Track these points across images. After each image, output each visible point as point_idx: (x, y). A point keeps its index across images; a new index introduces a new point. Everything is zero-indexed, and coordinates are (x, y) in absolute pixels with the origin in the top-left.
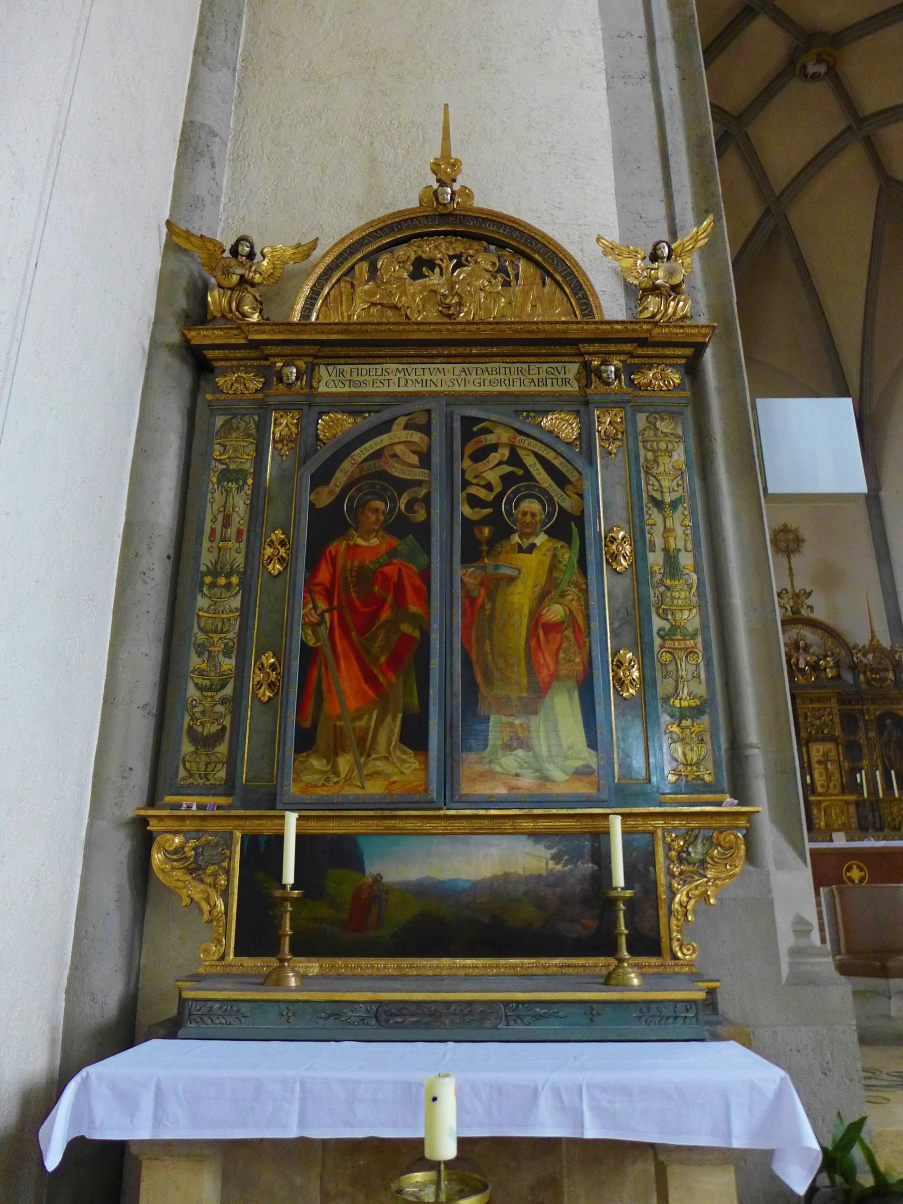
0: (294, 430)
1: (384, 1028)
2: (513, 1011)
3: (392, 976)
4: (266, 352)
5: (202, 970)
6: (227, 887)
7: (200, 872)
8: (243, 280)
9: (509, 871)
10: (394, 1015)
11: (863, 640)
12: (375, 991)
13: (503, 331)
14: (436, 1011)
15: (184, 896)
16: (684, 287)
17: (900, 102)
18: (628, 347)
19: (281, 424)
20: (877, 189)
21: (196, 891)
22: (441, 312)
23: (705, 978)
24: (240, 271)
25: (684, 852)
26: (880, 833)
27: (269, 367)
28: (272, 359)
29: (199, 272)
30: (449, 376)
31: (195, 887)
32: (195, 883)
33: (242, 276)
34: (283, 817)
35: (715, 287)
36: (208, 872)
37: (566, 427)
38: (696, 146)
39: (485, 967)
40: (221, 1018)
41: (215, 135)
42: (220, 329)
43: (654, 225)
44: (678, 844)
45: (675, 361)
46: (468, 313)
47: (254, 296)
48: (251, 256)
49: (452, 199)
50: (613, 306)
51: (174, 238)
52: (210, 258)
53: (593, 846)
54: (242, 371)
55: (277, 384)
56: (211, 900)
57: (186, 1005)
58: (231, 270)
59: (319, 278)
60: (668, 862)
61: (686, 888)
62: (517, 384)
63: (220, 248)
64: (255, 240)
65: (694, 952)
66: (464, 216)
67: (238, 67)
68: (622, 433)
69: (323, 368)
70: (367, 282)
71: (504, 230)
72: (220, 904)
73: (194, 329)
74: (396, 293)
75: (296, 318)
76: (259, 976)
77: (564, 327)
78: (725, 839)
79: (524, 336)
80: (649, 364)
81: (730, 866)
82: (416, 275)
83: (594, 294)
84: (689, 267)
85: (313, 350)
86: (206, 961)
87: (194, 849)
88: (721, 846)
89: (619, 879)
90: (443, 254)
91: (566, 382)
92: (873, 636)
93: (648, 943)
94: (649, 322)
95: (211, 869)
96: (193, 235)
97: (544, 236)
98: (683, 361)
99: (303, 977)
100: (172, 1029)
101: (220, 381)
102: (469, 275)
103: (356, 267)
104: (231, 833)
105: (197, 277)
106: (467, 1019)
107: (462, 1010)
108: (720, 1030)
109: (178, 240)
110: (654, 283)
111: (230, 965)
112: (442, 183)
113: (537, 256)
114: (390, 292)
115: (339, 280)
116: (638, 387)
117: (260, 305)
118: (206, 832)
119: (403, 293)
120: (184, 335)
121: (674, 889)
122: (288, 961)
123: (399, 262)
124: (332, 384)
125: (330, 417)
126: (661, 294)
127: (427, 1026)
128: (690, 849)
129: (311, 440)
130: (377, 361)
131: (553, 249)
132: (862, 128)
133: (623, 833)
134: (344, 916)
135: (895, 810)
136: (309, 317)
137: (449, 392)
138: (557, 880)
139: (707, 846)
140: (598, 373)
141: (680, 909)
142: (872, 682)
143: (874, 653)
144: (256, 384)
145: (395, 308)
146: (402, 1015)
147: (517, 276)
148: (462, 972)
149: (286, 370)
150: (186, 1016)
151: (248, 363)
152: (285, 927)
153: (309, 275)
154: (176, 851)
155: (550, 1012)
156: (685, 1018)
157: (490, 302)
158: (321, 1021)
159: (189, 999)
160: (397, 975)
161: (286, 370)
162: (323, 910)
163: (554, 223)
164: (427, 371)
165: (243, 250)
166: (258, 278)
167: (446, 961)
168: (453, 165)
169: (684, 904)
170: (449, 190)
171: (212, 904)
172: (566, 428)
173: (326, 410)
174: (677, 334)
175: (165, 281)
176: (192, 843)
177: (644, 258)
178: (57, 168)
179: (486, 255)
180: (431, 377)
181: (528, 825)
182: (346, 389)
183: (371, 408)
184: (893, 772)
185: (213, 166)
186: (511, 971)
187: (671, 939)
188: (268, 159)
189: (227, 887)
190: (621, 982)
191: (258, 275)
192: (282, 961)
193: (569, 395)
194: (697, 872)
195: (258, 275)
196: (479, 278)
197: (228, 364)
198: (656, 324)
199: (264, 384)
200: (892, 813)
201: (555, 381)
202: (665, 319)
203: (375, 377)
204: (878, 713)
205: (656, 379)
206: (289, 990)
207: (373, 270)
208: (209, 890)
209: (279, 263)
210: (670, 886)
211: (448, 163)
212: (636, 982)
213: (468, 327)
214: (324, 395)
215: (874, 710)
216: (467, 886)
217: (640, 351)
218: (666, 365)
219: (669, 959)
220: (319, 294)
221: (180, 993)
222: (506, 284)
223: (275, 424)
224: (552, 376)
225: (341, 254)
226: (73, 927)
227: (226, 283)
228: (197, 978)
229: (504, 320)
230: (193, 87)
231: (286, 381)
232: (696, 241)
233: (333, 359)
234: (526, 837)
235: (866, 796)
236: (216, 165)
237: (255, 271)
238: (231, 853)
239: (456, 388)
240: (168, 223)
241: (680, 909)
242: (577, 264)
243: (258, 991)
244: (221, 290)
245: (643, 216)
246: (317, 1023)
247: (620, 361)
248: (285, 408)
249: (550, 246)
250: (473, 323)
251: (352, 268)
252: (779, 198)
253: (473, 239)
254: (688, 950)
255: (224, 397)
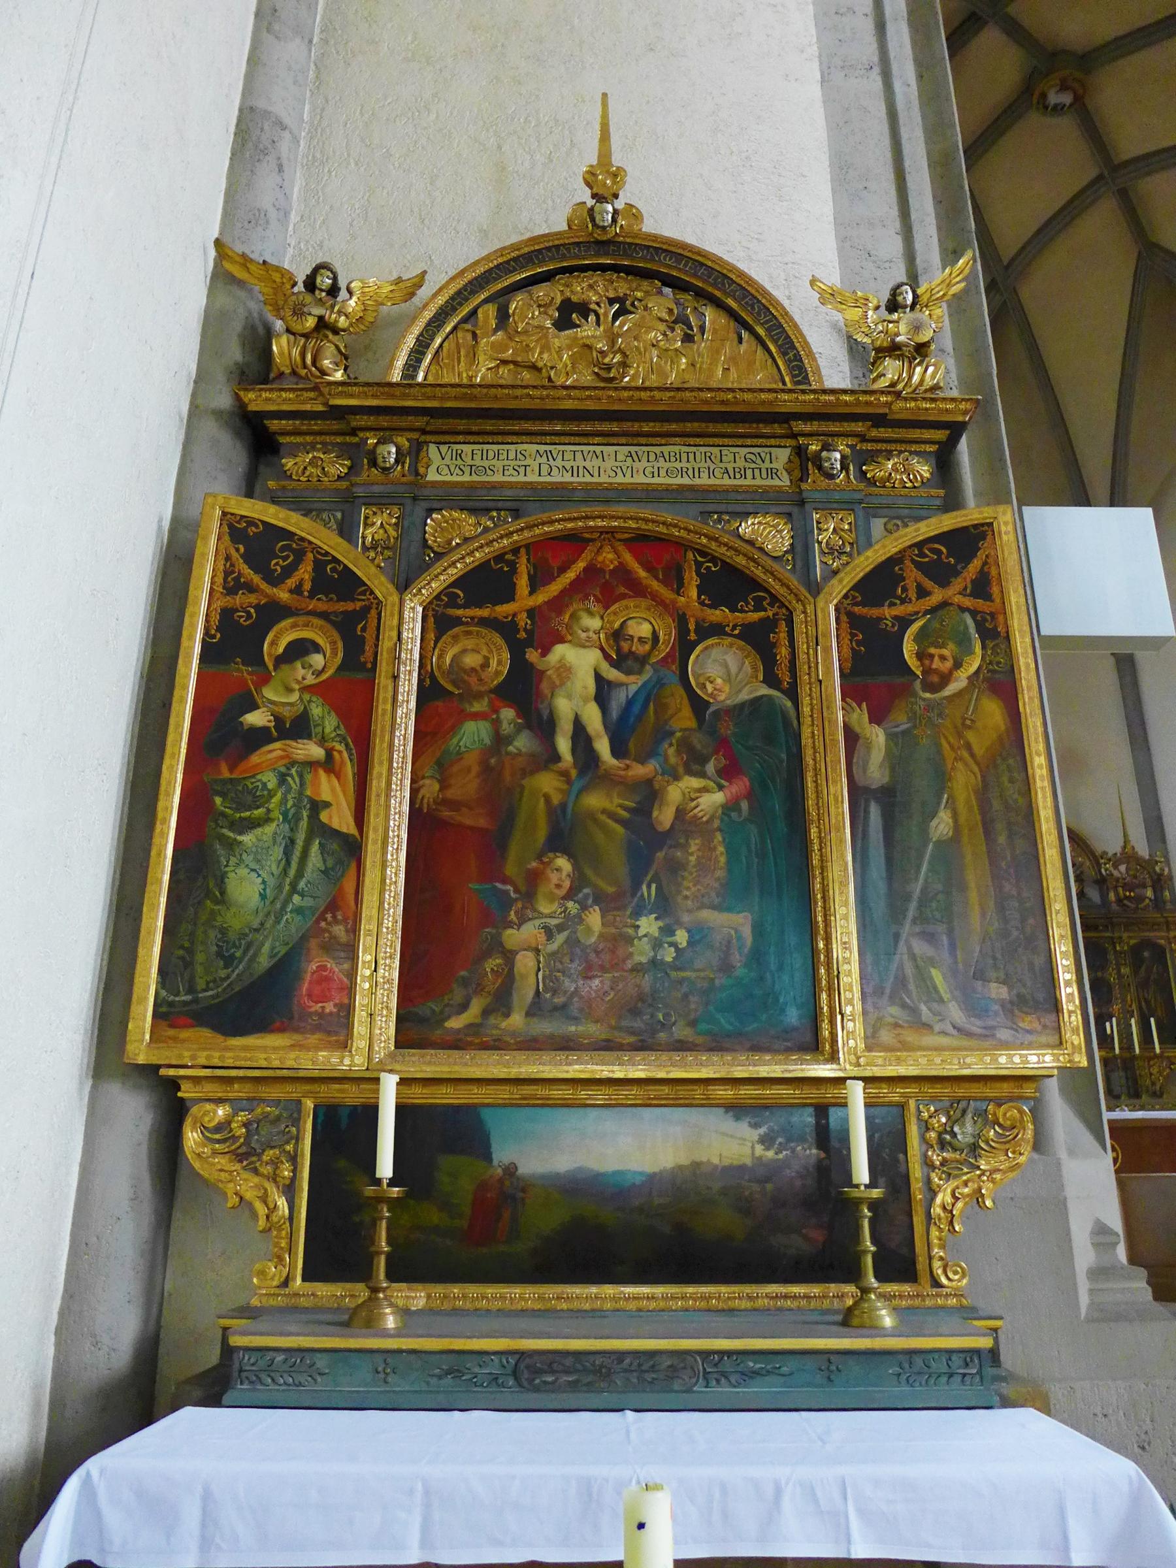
0: (393, 533)
1: (528, 1390)
2: (716, 1365)
3: (533, 1310)
4: (354, 424)
5: (255, 1302)
6: (293, 1179)
7: (254, 1159)
8: (322, 323)
9: (698, 1160)
10: (540, 1372)
11: (1113, 846)
12: (513, 1337)
13: (687, 402)
14: (601, 1366)
15: (230, 1193)
16: (933, 347)
17: (1171, 143)
18: (859, 427)
19: (373, 524)
20: (1136, 255)
21: (247, 1185)
22: (596, 374)
23: (981, 1313)
24: (318, 311)
25: (946, 1132)
26: (1136, 1101)
27: (357, 445)
28: (361, 435)
29: (260, 314)
30: (610, 463)
31: (245, 1180)
32: (246, 1175)
33: (321, 318)
34: (377, 1080)
35: (969, 355)
36: (265, 1158)
37: (770, 533)
38: (940, 165)
39: (665, 1298)
40: (285, 1375)
41: (284, 128)
42: (291, 390)
43: (887, 265)
44: (938, 1121)
45: (923, 447)
46: (633, 378)
47: (337, 347)
48: (333, 291)
49: (614, 220)
50: (834, 371)
51: (228, 265)
52: (275, 294)
53: (817, 1123)
54: (318, 450)
55: (369, 469)
56: (270, 1199)
57: (235, 1356)
58: (305, 310)
59: (429, 324)
60: (924, 1147)
61: (953, 1184)
62: (705, 475)
63: (291, 279)
64: (338, 266)
65: (963, 1277)
66: (630, 244)
67: (315, 40)
68: (851, 544)
69: (433, 448)
70: (495, 331)
71: (685, 265)
72: (282, 1203)
73: (253, 389)
74: (536, 346)
75: (396, 376)
76: (338, 1309)
77: (771, 396)
78: (1005, 1114)
79: (717, 408)
80: (886, 450)
81: (1014, 1153)
82: (563, 323)
83: (810, 354)
84: (935, 323)
85: (420, 422)
86: (260, 1288)
87: (245, 1125)
88: (1000, 1126)
89: (861, 1172)
90: (601, 296)
91: (772, 473)
92: (1126, 841)
93: (900, 1265)
94: (889, 393)
95: (269, 1155)
96: (252, 260)
97: (742, 274)
98: (932, 448)
99: (404, 1313)
100: (214, 1389)
101: (288, 463)
102: (638, 325)
103: (480, 311)
104: (299, 1102)
105: (257, 322)
106: (649, 1377)
107: (640, 1365)
108: (1006, 1389)
109: (230, 269)
110: (893, 341)
111: (296, 1295)
112: (599, 198)
113: (731, 302)
114: (527, 346)
115: (455, 328)
116: (872, 482)
117: (345, 358)
118: (263, 1100)
119: (546, 348)
120: (237, 397)
121: (935, 1187)
122: (384, 1290)
123: (539, 306)
124: (446, 471)
125: (443, 516)
126: (902, 355)
127: (590, 1387)
128: (956, 1129)
129: (415, 548)
130: (510, 439)
131: (753, 291)
132: (1116, 178)
133: (867, 1105)
134: (464, 1224)
135: (1155, 1070)
136: (414, 377)
137: (611, 484)
138: (764, 1173)
139: (979, 1125)
140: (817, 461)
141: (942, 1215)
142: (1126, 902)
143: (1128, 863)
144: (339, 468)
145: (534, 368)
146: (553, 1372)
147: (702, 329)
148: (632, 1306)
149: (382, 450)
150: (235, 1374)
151: (328, 439)
152: (380, 1242)
153: (414, 319)
154: (218, 1128)
155: (768, 1367)
156: (964, 1375)
157: (666, 363)
158: (434, 1381)
159: (239, 1348)
160: (539, 1310)
161: (382, 450)
162: (433, 1216)
163: (751, 260)
164: (579, 455)
165: (321, 283)
166: (343, 322)
167: (609, 1290)
168: (615, 175)
169: (949, 1208)
170: (610, 208)
171: (272, 1206)
172: (774, 537)
173: (436, 505)
174: (926, 409)
175: (212, 323)
176: (242, 1117)
177: (877, 308)
178: (65, 141)
179: (660, 300)
180: (584, 464)
181: (724, 1093)
182: (466, 478)
183: (500, 505)
184: (1152, 1020)
185: (280, 168)
186: (703, 1304)
187: (930, 1258)
188: (357, 164)
189: (293, 1179)
190: (868, 1322)
191: (343, 318)
192: (375, 1290)
193: (779, 490)
194: (965, 1162)
195: (343, 318)
196: (650, 329)
197: (299, 439)
198: (898, 394)
199: (350, 468)
200: (1151, 1074)
201: (757, 472)
202: (909, 390)
203: (506, 463)
204: (1132, 942)
205: (896, 471)
206: (385, 1334)
207: (503, 316)
208: (267, 1185)
209: (371, 304)
210: (928, 1181)
211: (608, 172)
212: (888, 1321)
213: (637, 394)
214: (434, 484)
215: (1129, 939)
216: (638, 1180)
217: (874, 433)
218: (911, 453)
219: (928, 1286)
220: (428, 346)
221: (225, 1339)
222: (688, 339)
223: (366, 525)
224: (753, 466)
225: (459, 293)
226: (68, 1238)
227: (298, 328)
228: (248, 1312)
229: (686, 386)
230: (254, 60)
231: (382, 465)
232: (949, 285)
233: (446, 436)
234: (721, 1110)
235: (1117, 1051)
236: (285, 168)
237: (340, 312)
238: (298, 1131)
239: (620, 479)
240: (218, 243)
241: (942, 1215)
242: (787, 313)
243: (342, 1336)
244: (292, 337)
245: (872, 253)
246: (428, 1383)
247: (847, 445)
248: (380, 502)
249: (749, 289)
250: (645, 389)
251: (474, 312)
252: (1007, 267)
253: (641, 277)
254: (956, 1273)
255: (294, 484)
